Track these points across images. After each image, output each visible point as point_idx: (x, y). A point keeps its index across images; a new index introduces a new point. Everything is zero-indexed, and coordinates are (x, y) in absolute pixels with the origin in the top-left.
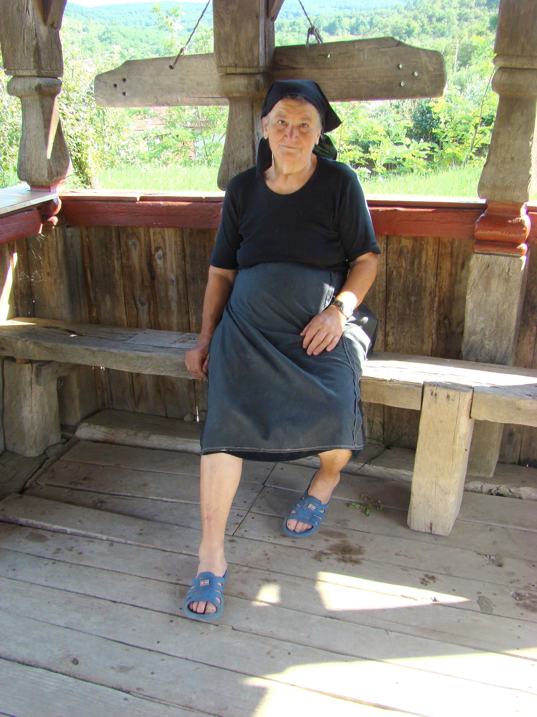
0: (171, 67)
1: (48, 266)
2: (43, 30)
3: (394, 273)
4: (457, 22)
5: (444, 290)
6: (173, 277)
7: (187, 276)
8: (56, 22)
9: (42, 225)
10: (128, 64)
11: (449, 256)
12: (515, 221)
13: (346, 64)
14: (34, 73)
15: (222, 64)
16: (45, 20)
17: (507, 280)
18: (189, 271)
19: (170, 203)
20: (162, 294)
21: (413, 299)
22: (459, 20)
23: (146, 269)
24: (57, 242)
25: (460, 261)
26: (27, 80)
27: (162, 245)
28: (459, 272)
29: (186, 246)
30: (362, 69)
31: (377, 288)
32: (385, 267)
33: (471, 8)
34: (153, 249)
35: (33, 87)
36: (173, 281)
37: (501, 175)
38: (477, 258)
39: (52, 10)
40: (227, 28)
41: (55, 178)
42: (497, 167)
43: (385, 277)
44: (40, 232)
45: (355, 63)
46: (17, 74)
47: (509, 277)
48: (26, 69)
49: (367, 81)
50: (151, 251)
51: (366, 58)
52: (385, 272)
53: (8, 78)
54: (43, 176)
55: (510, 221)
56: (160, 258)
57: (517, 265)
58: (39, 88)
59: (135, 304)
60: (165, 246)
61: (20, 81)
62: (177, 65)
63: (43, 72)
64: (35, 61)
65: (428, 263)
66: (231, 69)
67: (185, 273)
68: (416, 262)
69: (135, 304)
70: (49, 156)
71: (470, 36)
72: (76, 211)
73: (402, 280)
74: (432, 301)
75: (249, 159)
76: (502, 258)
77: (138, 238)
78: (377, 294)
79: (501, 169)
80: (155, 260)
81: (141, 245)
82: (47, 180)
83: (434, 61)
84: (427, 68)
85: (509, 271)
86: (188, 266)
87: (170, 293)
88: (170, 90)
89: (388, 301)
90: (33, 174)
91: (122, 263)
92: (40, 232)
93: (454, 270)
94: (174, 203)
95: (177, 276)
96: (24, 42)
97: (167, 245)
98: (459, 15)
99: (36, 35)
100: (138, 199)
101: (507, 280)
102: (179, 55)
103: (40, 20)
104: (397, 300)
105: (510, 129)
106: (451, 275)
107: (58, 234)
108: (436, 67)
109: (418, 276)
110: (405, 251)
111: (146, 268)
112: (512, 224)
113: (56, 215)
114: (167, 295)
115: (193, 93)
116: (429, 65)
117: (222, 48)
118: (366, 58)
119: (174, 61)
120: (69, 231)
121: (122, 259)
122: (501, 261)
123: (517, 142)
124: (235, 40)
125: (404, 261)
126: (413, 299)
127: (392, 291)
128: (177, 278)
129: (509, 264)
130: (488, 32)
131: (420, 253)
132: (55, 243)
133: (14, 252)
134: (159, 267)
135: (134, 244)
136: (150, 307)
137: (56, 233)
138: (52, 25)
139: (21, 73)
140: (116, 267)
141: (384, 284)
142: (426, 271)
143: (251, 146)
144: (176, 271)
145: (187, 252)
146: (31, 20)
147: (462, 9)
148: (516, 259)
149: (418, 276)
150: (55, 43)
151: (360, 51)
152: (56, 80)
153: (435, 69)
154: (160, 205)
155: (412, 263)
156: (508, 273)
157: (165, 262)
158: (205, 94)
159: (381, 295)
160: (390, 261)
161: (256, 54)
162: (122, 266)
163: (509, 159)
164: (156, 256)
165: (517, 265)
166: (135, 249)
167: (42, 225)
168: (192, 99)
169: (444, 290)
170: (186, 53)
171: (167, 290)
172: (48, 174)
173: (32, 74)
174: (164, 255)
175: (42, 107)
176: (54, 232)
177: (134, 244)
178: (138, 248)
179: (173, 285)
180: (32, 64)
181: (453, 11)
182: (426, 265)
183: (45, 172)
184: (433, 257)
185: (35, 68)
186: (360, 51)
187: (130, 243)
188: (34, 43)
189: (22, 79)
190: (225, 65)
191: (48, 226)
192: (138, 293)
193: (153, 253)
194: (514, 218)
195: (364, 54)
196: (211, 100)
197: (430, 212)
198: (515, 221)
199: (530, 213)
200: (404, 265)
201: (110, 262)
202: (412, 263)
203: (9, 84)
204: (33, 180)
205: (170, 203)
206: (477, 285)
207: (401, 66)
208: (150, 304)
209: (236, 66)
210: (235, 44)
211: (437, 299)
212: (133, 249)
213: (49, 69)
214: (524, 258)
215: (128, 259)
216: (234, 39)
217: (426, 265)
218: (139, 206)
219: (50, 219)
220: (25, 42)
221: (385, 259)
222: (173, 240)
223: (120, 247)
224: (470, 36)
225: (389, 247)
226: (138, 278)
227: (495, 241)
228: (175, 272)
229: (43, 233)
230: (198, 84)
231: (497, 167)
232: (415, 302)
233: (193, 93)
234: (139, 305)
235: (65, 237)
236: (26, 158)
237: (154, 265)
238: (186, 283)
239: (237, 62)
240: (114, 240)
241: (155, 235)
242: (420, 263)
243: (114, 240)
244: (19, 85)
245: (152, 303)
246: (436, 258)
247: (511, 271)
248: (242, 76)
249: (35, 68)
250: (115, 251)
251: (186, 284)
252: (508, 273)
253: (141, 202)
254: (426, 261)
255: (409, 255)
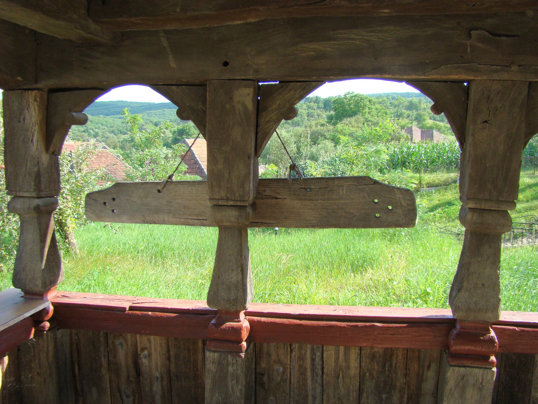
0: (159, 191)
1: (38, 366)
2: (45, 158)
3: (367, 374)
4: (306, 118)
5: (413, 388)
6: (157, 374)
7: (172, 375)
8: (57, 150)
9: (33, 330)
10: (118, 185)
11: (417, 359)
12: (486, 337)
13: (326, 197)
14: (34, 194)
15: (215, 197)
16: (47, 150)
17: (480, 389)
18: (173, 370)
19: (158, 314)
20: (147, 389)
21: (384, 396)
22: (308, 116)
23: (132, 366)
24: (48, 345)
25: (427, 364)
26: (27, 200)
27: (148, 345)
28: (425, 373)
29: (171, 348)
30: (341, 201)
31: (352, 387)
32: (359, 370)
33: (315, 110)
34: (139, 349)
35: (32, 207)
36: (158, 378)
37: (474, 299)
38: (453, 371)
39: (55, 141)
40: (220, 166)
41: (48, 287)
42: (470, 291)
43: (359, 378)
44: (32, 336)
45: (334, 196)
46: (18, 195)
47: (483, 386)
48: (26, 191)
49: (347, 213)
50: (136, 351)
51: (345, 193)
52: (359, 374)
53: (9, 198)
54: (37, 286)
55: (482, 338)
56: (146, 358)
57: (489, 377)
58: (37, 209)
59: (121, 396)
60: (150, 347)
61: (20, 201)
62: (165, 189)
63: (42, 193)
64: (35, 185)
65: (398, 365)
66: (222, 201)
67: (169, 371)
68: (387, 365)
69: (121, 396)
70: (43, 267)
71: (316, 126)
72: (66, 313)
73: (374, 381)
74: (402, 397)
75: (238, 281)
76: (476, 370)
77: (125, 339)
78: (351, 392)
79: (473, 293)
80: (141, 359)
81: (127, 345)
82: (41, 290)
83: (408, 197)
84: (401, 203)
85: (482, 381)
86: (172, 366)
87: (155, 388)
88: (157, 211)
89: (362, 398)
90: (27, 283)
91: (109, 360)
92: (32, 336)
93: (421, 371)
94: (163, 314)
95: (161, 373)
96: (26, 168)
97: (153, 347)
98: (308, 113)
99: (38, 163)
100: (128, 309)
101: (480, 389)
102: (167, 181)
103: (43, 150)
104: (370, 397)
105: (479, 259)
106: (418, 375)
107: (49, 338)
108: (409, 202)
109: (389, 376)
110: (377, 356)
111: (131, 366)
112: (484, 340)
113: (48, 321)
114: (151, 390)
115: (179, 214)
116: (402, 201)
117: (215, 183)
118: (345, 193)
119: (163, 186)
120: (60, 333)
121: (108, 357)
122: (476, 372)
123: (486, 270)
124: (227, 177)
125: (376, 364)
126: (384, 396)
127: (365, 390)
128: (162, 376)
129: (482, 376)
130: (327, 124)
131: (391, 357)
132: (46, 346)
133: (5, 356)
134: (144, 365)
135: (121, 344)
136: (134, 400)
137: (47, 337)
138: (53, 153)
139: (21, 194)
140: (103, 363)
141: (358, 384)
142: (396, 373)
143: (240, 269)
144: (161, 369)
145: (172, 353)
146: (34, 150)
147: (309, 110)
148: (489, 370)
149: (389, 376)
150: (55, 167)
151: (339, 186)
152: (53, 198)
153: (408, 205)
154: (149, 315)
155: (384, 366)
156: (481, 383)
157: (150, 361)
158: (191, 215)
159: (355, 393)
160: (363, 364)
161: (248, 190)
162: (109, 363)
163: (481, 285)
164: (142, 355)
165: (489, 377)
166: (122, 348)
167: (33, 330)
168: (178, 220)
169: (413, 388)
170: (174, 179)
171: (151, 385)
172: (42, 284)
173: (32, 196)
174: (150, 355)
175: (39, 223)
176: (45, 337)
177: (121, 344)
178: (124, 348)
179: (157, 381)
180: (33, 187)
181: (304, 111)
182: (396, 367)
183: (39, 282)
184: (403, 360)
185: (35, 191)
186: (339, 186)
187: (117, 342)
188: (36, 169)
189: (22, 200)
190: (217, 198)
191: (39, 332)
192: (123, 387)
193: (139, 352)
194: (485, 335)
195: (343, 190)
196: (196, 221)
197: (405, 327)
198: (486, 337)
199: (493, 326)
200: (376, 367)
201: (97, 358)
202: (384, 366)
203: (9, 204)
204: (28, 288)
205: (158, 314)
206: (453, 393)
207: (376, 201)
208: (135, 397)
209: (227, 199)
210: (228, 180)
211: (406, 396)
212: (120, 349)
213: (48, 190)
214: (495, 369)
215: (115, 357)
216: (227, 176)
217: (396, 367)
218: (128, 315)
219: (42, 324)
220: (28, 167)
221: (359, 363)
222: (159, 342)
223: (108, 346)
224: (316, 126)
225: (363, 352)
226: (124, 374)
227: (467, 355)
228: (160, 370)
229: (35, 336)
230: (185, 207)
231: (470, 291)
232: (386, 398)
233: (179, 214)
234: (124, 397)
235: (55, 339)
236: (22, 269)
237: (140, 363)
238: (170, 380)
239: (229, 195)
240: (102, 339)
241: (142, 340)
242: (391, 366)
243: (102, 339)
244: (19, 204)
245: (137, 395)
246: (405, 361)
247: (485, 381)
248: (233, 208)
249: (35, 191)
250: (102, 349)
251: (170, 382)
252: (481, 383)
253: (130, 312)
254: (396, 365)
255: (381, 359)
